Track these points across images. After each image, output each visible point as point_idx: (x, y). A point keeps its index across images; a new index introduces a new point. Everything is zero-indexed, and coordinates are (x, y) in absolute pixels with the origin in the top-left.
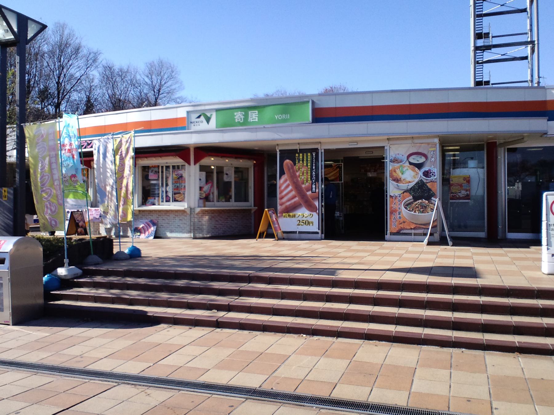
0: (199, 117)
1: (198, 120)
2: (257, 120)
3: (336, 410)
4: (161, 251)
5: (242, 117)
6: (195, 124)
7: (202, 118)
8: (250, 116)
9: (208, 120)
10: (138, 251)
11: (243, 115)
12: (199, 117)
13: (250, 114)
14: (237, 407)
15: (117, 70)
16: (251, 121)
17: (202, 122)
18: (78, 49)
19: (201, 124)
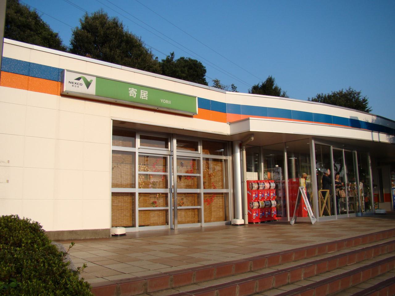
0: (79, 79)
1: (77, 81)
2: (147, 99)
3: (126, 283)
4: (312, 214)
5: (136, 93)
6: (74, 85)
7: (82, 81)
8: (141, 94)
9: (88, 84)
10: (333, 215)
11: (136, 92)
12: (79, 79)
13: (141, 92)
14: (82, 263)
15: (316, 98)
16: (142, 98)
17: (81, 84)
18: (359, 94)
19: (79, 86)
